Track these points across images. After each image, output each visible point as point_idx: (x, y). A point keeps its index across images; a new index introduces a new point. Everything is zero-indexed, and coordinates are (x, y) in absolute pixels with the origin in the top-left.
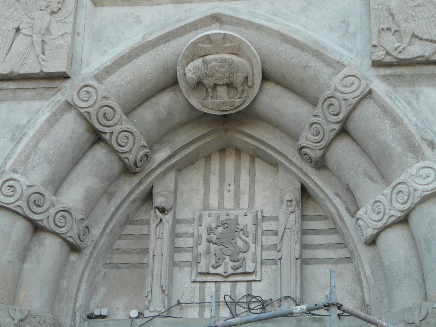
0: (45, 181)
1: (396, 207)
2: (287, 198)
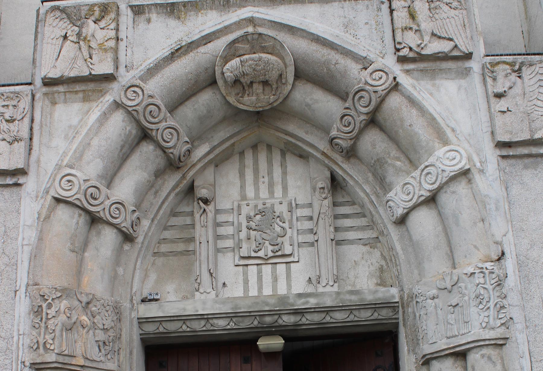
0: (99, 175)
1: (425, 188)
2: (320, 185)
